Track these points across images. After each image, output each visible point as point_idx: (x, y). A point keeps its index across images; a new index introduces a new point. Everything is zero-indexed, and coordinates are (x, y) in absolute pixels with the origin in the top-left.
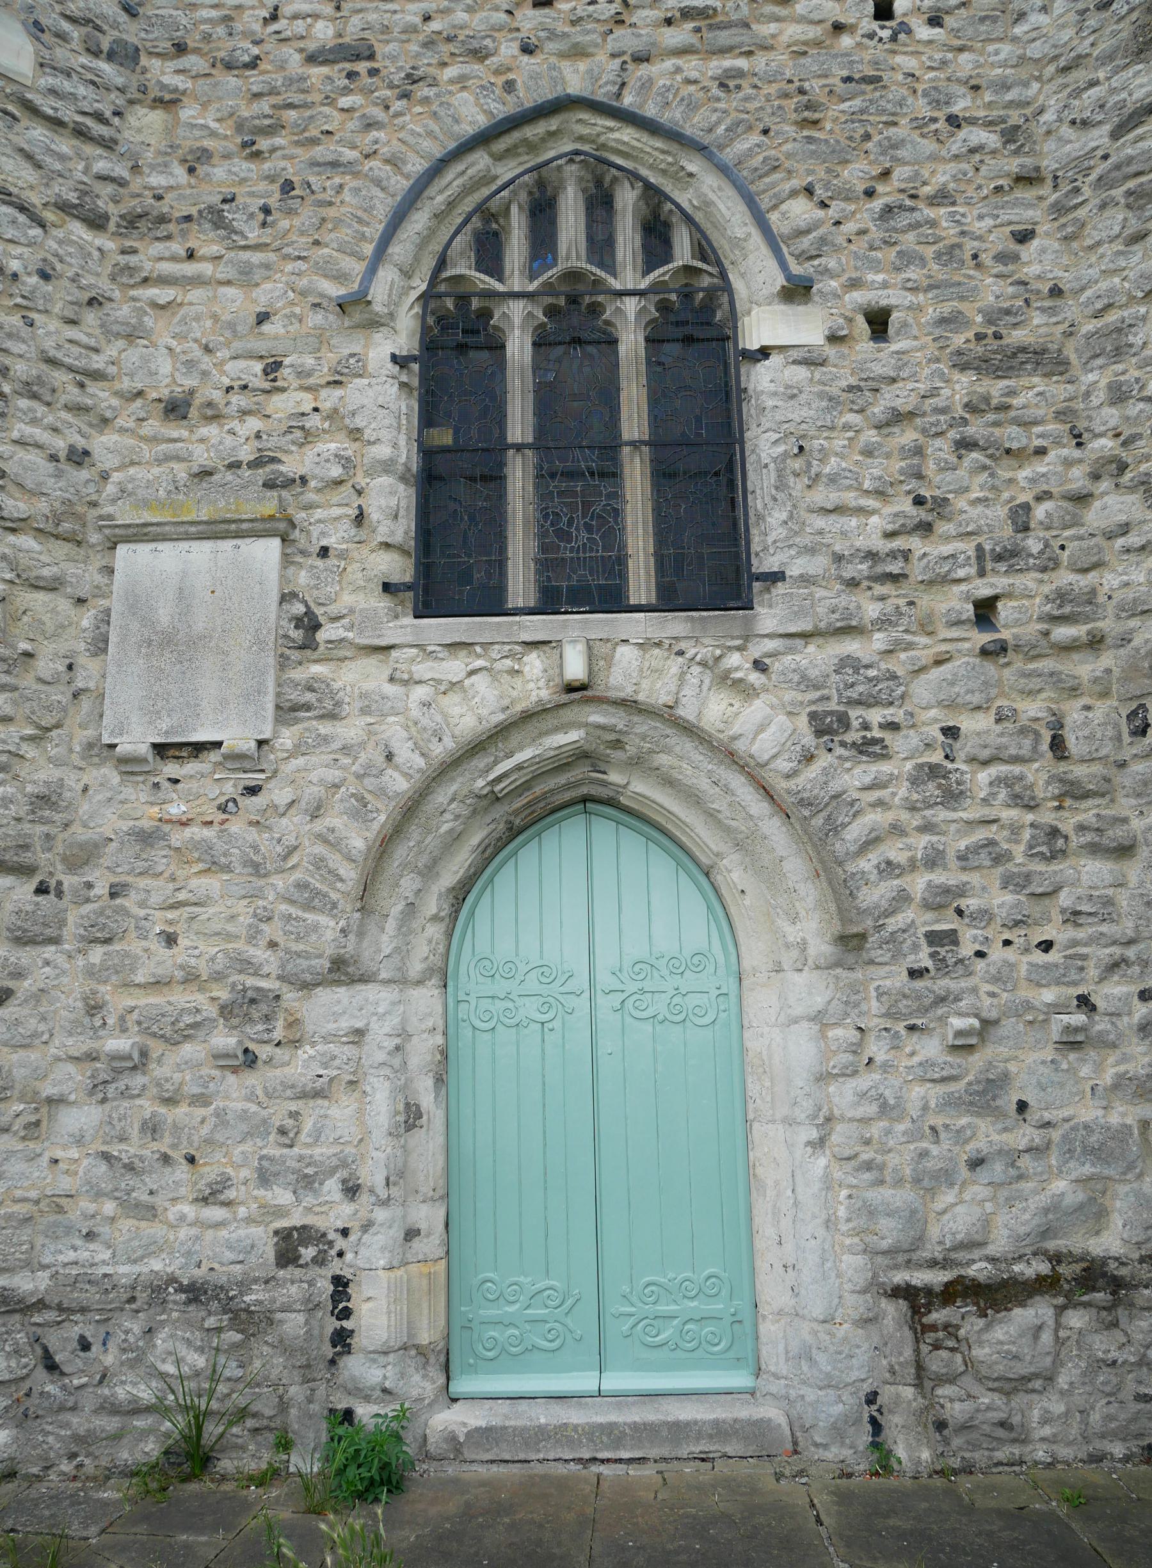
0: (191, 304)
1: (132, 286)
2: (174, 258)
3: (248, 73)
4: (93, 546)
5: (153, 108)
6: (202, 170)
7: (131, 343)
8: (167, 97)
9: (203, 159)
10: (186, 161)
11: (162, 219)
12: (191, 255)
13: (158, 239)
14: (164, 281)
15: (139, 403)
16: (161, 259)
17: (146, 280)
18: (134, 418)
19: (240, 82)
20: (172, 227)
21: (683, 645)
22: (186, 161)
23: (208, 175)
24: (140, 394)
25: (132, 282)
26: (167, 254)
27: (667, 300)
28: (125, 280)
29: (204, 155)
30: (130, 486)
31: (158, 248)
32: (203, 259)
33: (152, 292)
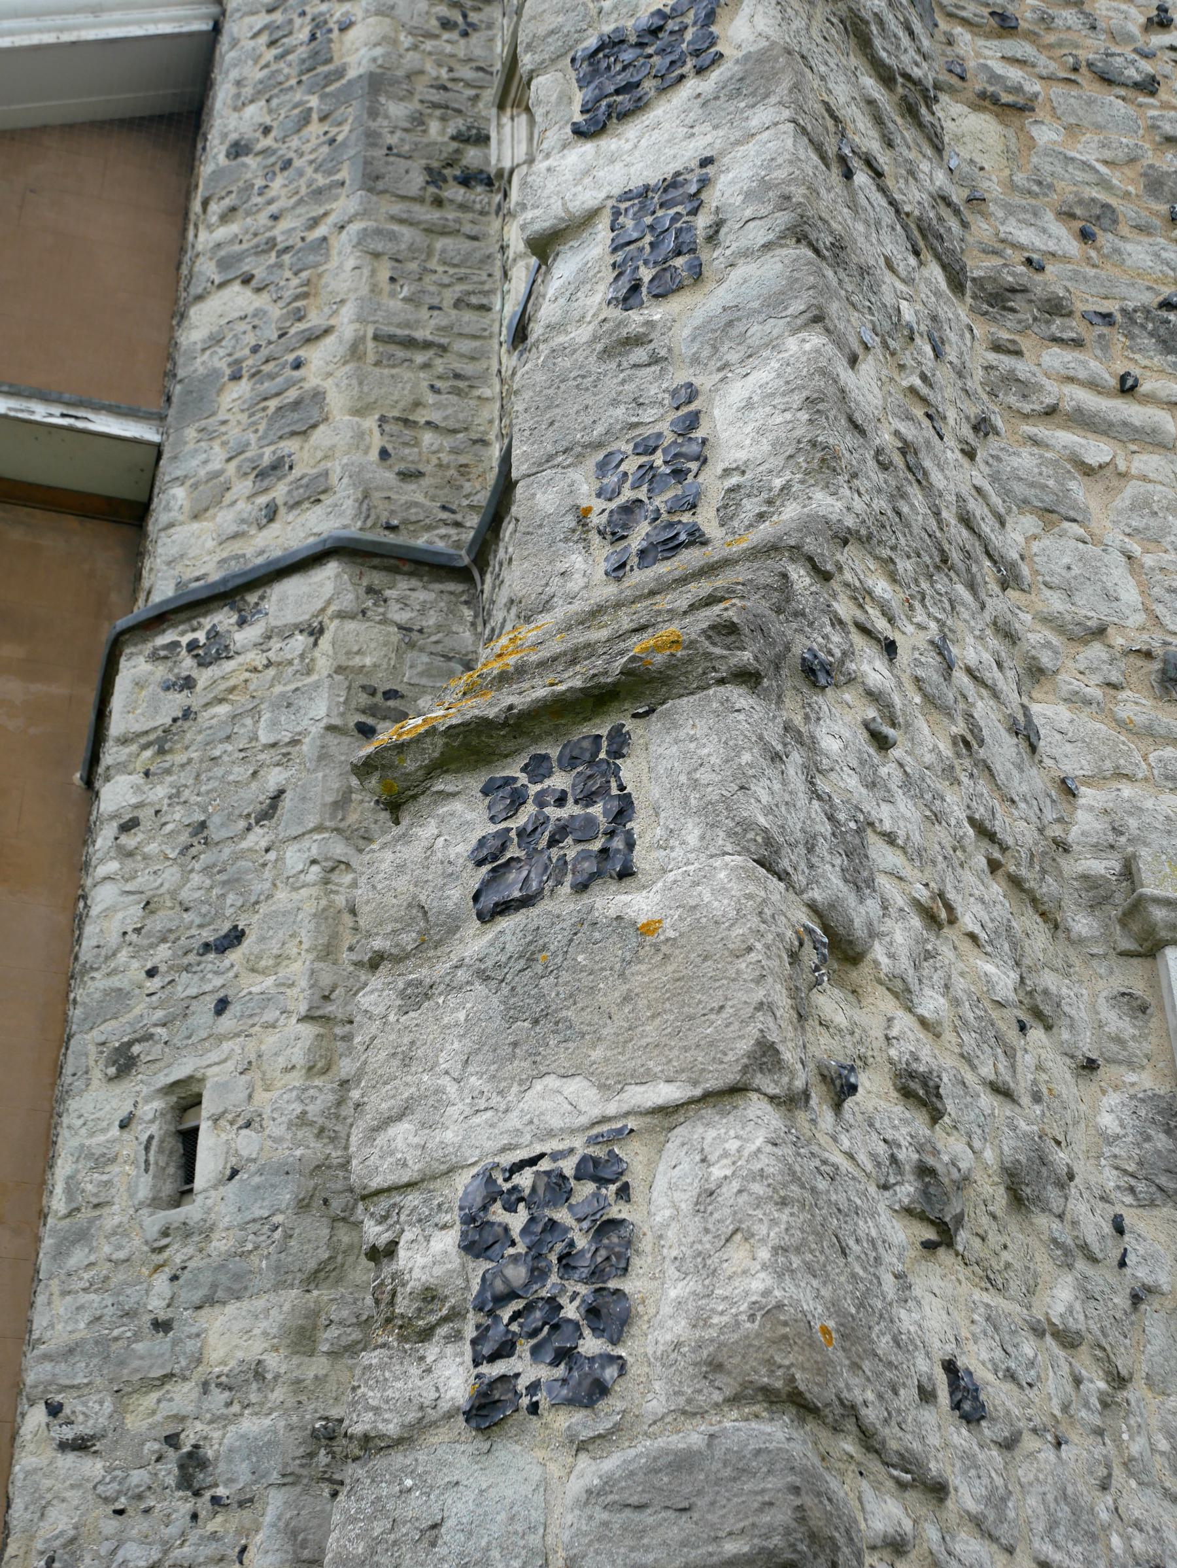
0: (1144, 478)
1: (1026, 416)
2: (1093, 385)
3: (1142, 99)
4: (1080, 941)
5: (976, 108)
6: (1105, 239)
7: (1048, 527)
8: (1006, 98)
9: (1106, 222)
10: (1072, 216)
11: (1055, 308)
12: (1127, 387)
13: (1055, 340)
14: (1083, 421)
15: (1096, 651)
16: (1071, 380)
17: (1051, 412)
18: (1097, 679)
19: (1131, 111)
20: (1075, 327)
21: (117, 1434)
22: (1072, 216)
23: (1117, 251)
24: (1100, 632)
25: (1027, 408)
26: (1082, 374)
27: (560, 759)
28: (1012, 400)
29: (1106, 215)
30: (1133, 823)
31: (1056, 358)
32: (1150, 399)
33: (1064, 438)
